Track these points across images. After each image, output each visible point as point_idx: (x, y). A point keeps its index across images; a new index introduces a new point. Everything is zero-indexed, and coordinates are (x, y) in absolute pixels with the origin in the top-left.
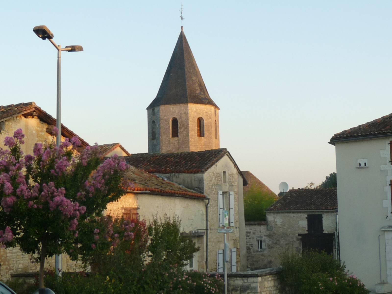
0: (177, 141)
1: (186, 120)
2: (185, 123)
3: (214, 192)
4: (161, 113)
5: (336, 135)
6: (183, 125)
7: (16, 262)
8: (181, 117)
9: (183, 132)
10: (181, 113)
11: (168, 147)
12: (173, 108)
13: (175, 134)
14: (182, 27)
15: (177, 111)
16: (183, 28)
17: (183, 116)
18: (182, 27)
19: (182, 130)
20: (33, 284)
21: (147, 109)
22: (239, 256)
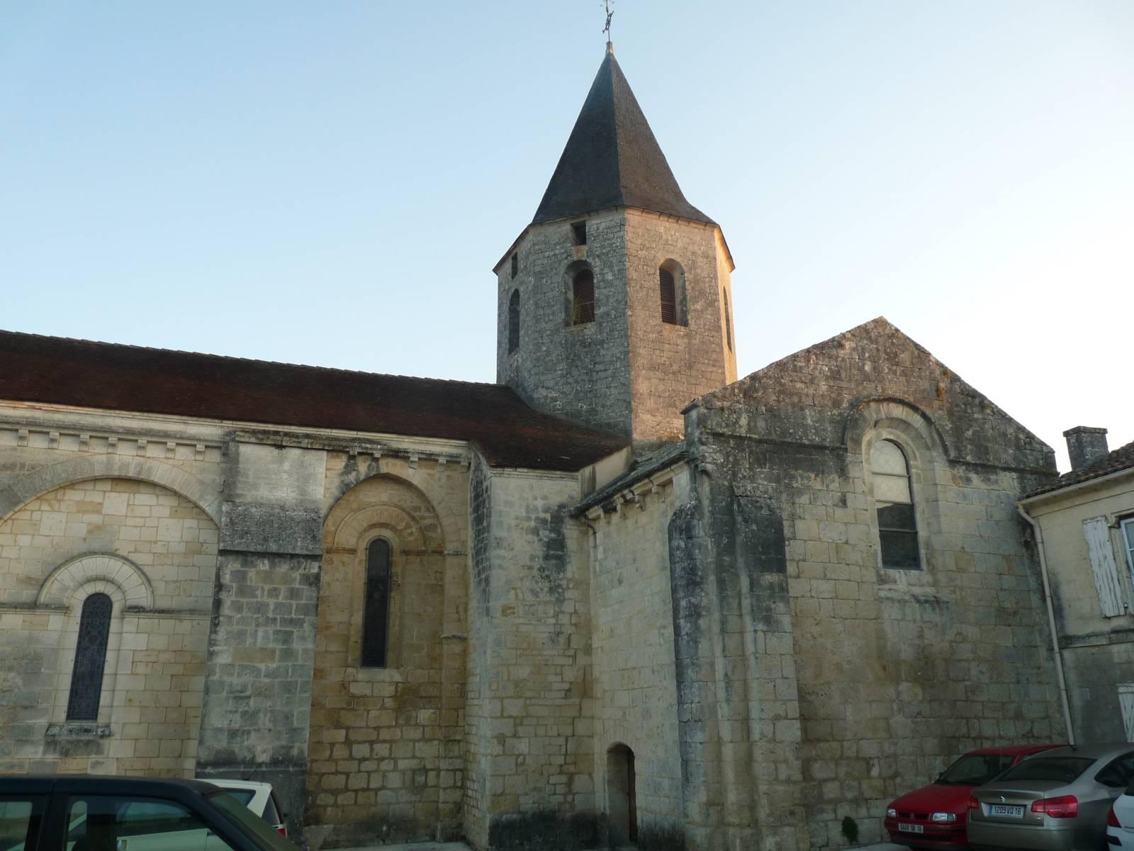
0: (683, 337)
1: (709, 276)
2: (707, 285)
3: (267, 529)
4: (629, 233)
5: (1079, 427)
6: (702, 293)
7: (344, 776)
8: (693, 266)
9: (702, 311)
10: (693, 253)
11: (657, 352)
12: (667, 230)
13: (672, 312)
14: (609, 44)
15: (680, 244)
16: (614, 46)
17: (701, 262)
18: (609, 44)
19: (698, 306)
20: (293, 757)
21: (496, 270)
22: (634, 668)
